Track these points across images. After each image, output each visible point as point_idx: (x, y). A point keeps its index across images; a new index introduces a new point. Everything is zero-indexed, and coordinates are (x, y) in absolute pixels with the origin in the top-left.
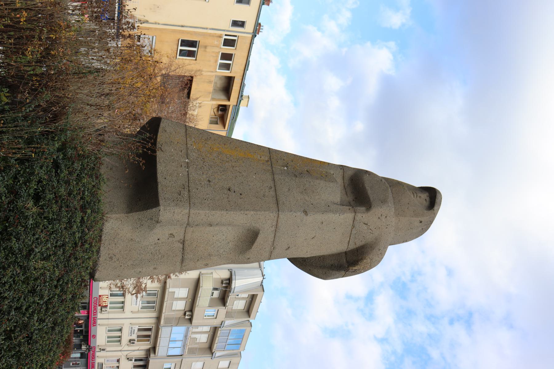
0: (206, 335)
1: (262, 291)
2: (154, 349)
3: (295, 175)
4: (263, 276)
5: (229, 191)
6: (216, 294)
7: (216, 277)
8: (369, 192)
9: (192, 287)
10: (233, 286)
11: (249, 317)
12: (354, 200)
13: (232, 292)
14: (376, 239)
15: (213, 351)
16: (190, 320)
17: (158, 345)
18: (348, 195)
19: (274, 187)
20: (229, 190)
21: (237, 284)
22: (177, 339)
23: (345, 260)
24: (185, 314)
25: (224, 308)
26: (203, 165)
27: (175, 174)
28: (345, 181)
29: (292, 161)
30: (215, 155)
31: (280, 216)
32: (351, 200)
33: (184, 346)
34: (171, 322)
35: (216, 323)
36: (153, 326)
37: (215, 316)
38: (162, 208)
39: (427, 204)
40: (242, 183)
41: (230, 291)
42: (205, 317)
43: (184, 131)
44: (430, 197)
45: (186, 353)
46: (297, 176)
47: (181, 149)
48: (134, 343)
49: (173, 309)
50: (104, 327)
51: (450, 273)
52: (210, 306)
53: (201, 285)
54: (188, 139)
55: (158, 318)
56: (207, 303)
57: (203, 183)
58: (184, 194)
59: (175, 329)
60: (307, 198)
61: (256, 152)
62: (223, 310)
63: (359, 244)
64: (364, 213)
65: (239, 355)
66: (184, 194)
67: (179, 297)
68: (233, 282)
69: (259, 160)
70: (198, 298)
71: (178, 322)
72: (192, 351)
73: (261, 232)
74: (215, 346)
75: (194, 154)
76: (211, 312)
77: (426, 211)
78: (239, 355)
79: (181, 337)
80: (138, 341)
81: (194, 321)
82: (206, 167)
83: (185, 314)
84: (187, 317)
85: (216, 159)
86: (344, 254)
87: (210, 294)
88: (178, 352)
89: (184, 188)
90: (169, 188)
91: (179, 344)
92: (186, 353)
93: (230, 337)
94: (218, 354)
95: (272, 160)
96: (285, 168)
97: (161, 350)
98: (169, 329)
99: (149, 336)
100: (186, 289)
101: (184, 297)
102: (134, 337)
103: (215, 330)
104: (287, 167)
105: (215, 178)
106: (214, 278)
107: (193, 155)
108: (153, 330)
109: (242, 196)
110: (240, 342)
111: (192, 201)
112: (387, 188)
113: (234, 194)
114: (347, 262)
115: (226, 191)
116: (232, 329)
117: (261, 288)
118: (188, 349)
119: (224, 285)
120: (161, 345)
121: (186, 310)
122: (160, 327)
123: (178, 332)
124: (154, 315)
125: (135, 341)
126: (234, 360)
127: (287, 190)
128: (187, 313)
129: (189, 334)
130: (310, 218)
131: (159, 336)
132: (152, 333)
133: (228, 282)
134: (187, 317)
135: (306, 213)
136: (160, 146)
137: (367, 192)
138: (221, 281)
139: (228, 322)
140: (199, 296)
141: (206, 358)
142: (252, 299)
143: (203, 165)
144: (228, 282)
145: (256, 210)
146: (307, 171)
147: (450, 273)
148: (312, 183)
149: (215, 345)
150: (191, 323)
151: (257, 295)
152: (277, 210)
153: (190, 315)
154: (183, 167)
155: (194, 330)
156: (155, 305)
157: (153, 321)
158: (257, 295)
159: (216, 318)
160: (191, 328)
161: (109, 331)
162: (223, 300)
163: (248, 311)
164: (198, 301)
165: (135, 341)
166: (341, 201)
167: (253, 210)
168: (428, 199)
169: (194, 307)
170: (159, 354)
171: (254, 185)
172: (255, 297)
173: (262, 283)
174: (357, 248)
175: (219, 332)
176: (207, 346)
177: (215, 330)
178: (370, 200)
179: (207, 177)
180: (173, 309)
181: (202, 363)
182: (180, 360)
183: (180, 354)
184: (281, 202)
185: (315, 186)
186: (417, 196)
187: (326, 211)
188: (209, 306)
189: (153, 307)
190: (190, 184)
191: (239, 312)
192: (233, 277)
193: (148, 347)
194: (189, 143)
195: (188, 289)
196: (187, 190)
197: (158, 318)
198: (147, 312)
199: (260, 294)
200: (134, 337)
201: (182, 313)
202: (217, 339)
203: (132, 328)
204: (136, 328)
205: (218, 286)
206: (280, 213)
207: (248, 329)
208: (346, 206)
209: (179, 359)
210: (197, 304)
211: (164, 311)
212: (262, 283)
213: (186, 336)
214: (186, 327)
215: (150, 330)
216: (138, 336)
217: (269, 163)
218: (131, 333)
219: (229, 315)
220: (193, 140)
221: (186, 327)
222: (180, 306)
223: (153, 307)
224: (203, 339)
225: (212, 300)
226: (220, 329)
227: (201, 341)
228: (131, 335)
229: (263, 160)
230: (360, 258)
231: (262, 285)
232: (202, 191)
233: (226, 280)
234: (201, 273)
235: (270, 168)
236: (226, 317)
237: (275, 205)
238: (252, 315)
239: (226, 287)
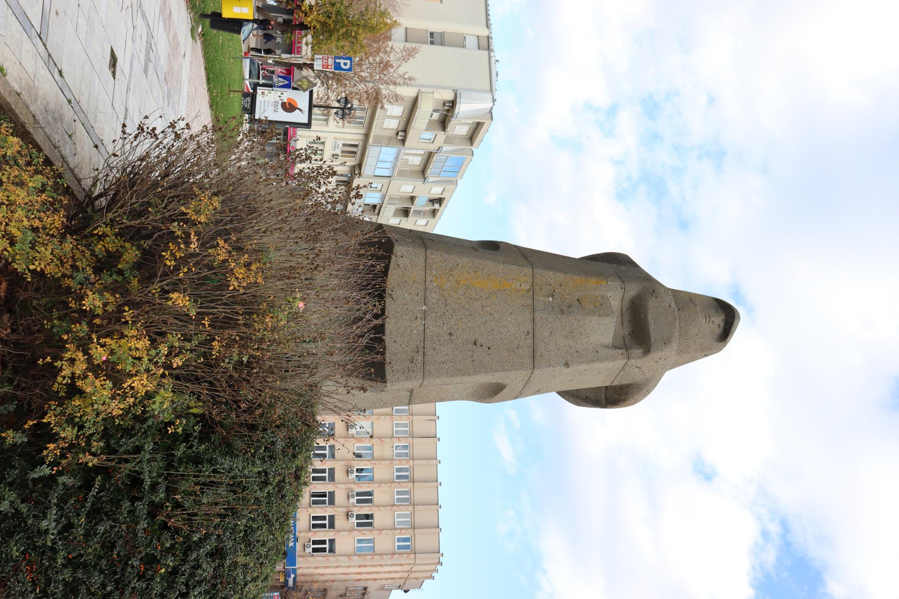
0: (420, 158)
1: (490, 118)
2: (360, 166)
3: (562, 310)
4: (494, 101)
5: (474, 346)
6: (436, 116)
7: (437, 98)
8: (652, 328)
9: (408, 105)
10: (457, 110)
11: (472, 144)
12: (630, 334)
13: (454, 117)
14: (647, 380)
15: (426, 176)
16: (403, 141)
17: (364, 164)
18: (624, 325)
19: (532, 332)
20: (475, 343)
21: (462, 108)
22: (386, 160)
23: (604, 396)
24: (397, 134)
25: (444, 133)
26: (445, 311)
27: (408, 332)
28: (624, 303)
29: (561, 285)
30: (461, 292)
31: (534, 372)
32: (627, 333)
33: (394, 168)
34: (379, 141)
35: (432, 148)
36: (360, 144)
37: (432, 141)
38: (388, 384)
39: (718, 331)
40: (492, 330)
41: (452, 116)
42: (420, 140)
43: (423, 260)
44: (725, 322)
45: (396, 175)
46: (565, 312)
47: (418, 291)
48: (337, 158)
49: (384, 127)
50: (305, 139)
51: (712, 100)
52: (428, 129)
53: (419, 106)
54: (428, 273)
55: (367, 136)
56: (424, 126)
57: (442, 339)
58: (418, 360)
59: (384, 149)
60: (572, 344)
61: (516, 277)
62: (441, 135)
63: (624, 382)
64: (639, 358)
65: (455, 182)
66: (418, 360)
67: (393, 115)
68: (458, 106)
69: (518, 291)
70: (414, 120)
71: (389, 142)
72: (402, 174)
73: (508, 387)
74: (429, 172)
75: (434, 296)
76: (429, 135)
77: (715, 343)
78: (456, 183)
79: (391, 158)
80: (342, 156)
81: (407, 144)
82: (447, 313)
83: (397, 134)
84: (399, 138)
85: (462, 299)
86: (604, 389)
87: (430, 114)
88: (386, 173)
89: (418, 352)
90: (399, 355)
91: (389, 165)
92: (396, 175)
93: (446, 164)
94: (431, 179)
95: (535, 287)
96: (551, 299)
97: (367, 169)
98: (379, 149)
99: (355, 153)
100: (400, 107)
101: (398, 115)
102: (338, 152)
103: (430, 155)
104: (553, 296)
105: (458, 329)
106: (436, 99)
107: (433, 297)
108: (360, 147)
109: (490, 351)
110: (458, 170)
111: (427, 367)
112: (675, 319)
113: (480, 349)
114: (606, 399)
115: (470, 346)
116: (450, 156)
117: (489, 116)
118: (399, 170)
119: (446, 108)
120: (367, 164)
121: (399, 130)
122: (368, 146)
123: (388, 153)
124: (363, 131)
125: (338, 156)
126: (449, 187)
127: (549, 334)
128: (400, 134)
129: (401, 156)
130: (570, 369)
131: (366, 155)
132: (359, 151)
133: (451, 105)
134: (399, 138)
135: (567, 365)
136: (391, 293)
137: (649, 328)
138: (442, 103)
139: (446, 148)
140: (415, 117)
141: (416, 182)
142: (478, 126)
143: (445, 311)
144: (451, 105)
145: (506, 371)
146: (578, 300)
147: (712, 100)
148: (582, 321)
149: (429, 170)
150: (404, 145)
151: (484, 123)
152: (532, 367)
153: (403, 136)
154: (419, 319)
155: (407, 152)
156: (363, 121)
157: (361, 137)
158: (484, 123)
159: (433, 142)
160: (403, 151)
161: (313, 496)
162: (443, 123)
163: (471, 138)
164: (414, 122)
165: (338, 156)
166: (613, 342)
167: (501, 371)
168: (722, 324)
169: (408, 127)
170: (365, 173)
171: (507, 332)
172: (480, 126)
173: (491, 109)
174: (621, 386)
175: (435, 158)
176: (420, 168)
177: (430, 155)
178: (650, 341)
179: (448, 329)
180: (384, 127)
181: (413, 187)
182: (388, 181)
183: (388, 175)
184: (538, 354)
185: (585, 326)
186: (709, 321)
187: (593, 360)
188: (426, 130)
189: (361, 123)
190: (426, 343)
191: (461, 138)
192: (458, 100)
193: (353, 164)
194: (429, 278)
195: (403, 107)
196: (421, 353)
197: (367, 136)
198: (353, 128)
199: (487, 122)
200: (338, 152)
201: (395, 132)
202: (432, 164)
203: (336, 142)
204: (340, 143)
205: (440, 107)
206: (535, 370)
207: (469, 157)
208: (619, 349)
209: (387, 180)
210: (412, 126)
211: (373, 129)
212: (491, 109)
213: (397, 158)
214: (397, 149)
215: (356, 146)
216: (343, 152)
217: (531, 293)
218: (335, 147)
219: (448, 141)
220: (435, 272)
221: (397, 149)
222: (393, 124)
223: (361, 123)
224: (417, 161)
225: (430, 122)
226: (436, 155)
227: (414, 163)
228: (335, 150)
229: (523, 290)
230: (623, 398)
231: (491, 112)
232: (441, 352)
233: (449, 102)
234: (420, 90)
235: (531, 302)
236: (444, 143)
237: (531, 360)
238: (475, 144)
239: (448, 111)
